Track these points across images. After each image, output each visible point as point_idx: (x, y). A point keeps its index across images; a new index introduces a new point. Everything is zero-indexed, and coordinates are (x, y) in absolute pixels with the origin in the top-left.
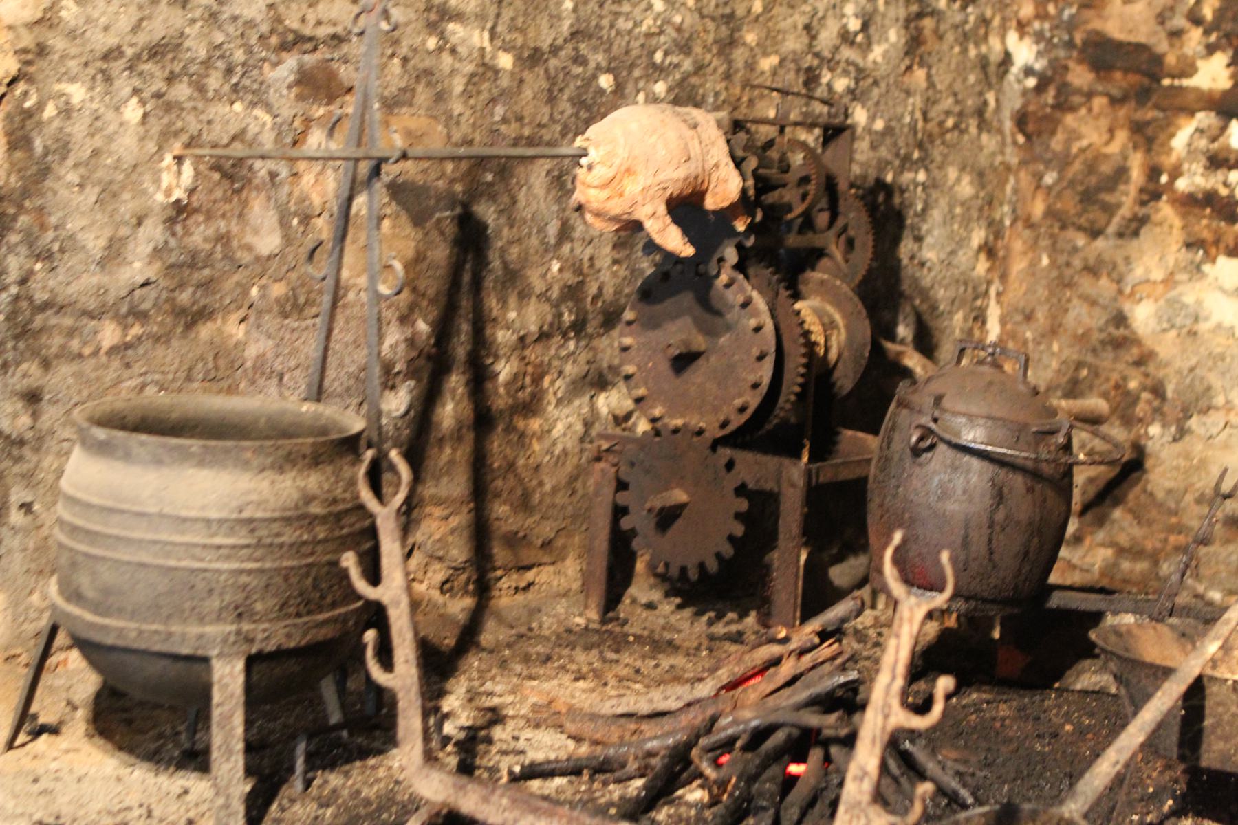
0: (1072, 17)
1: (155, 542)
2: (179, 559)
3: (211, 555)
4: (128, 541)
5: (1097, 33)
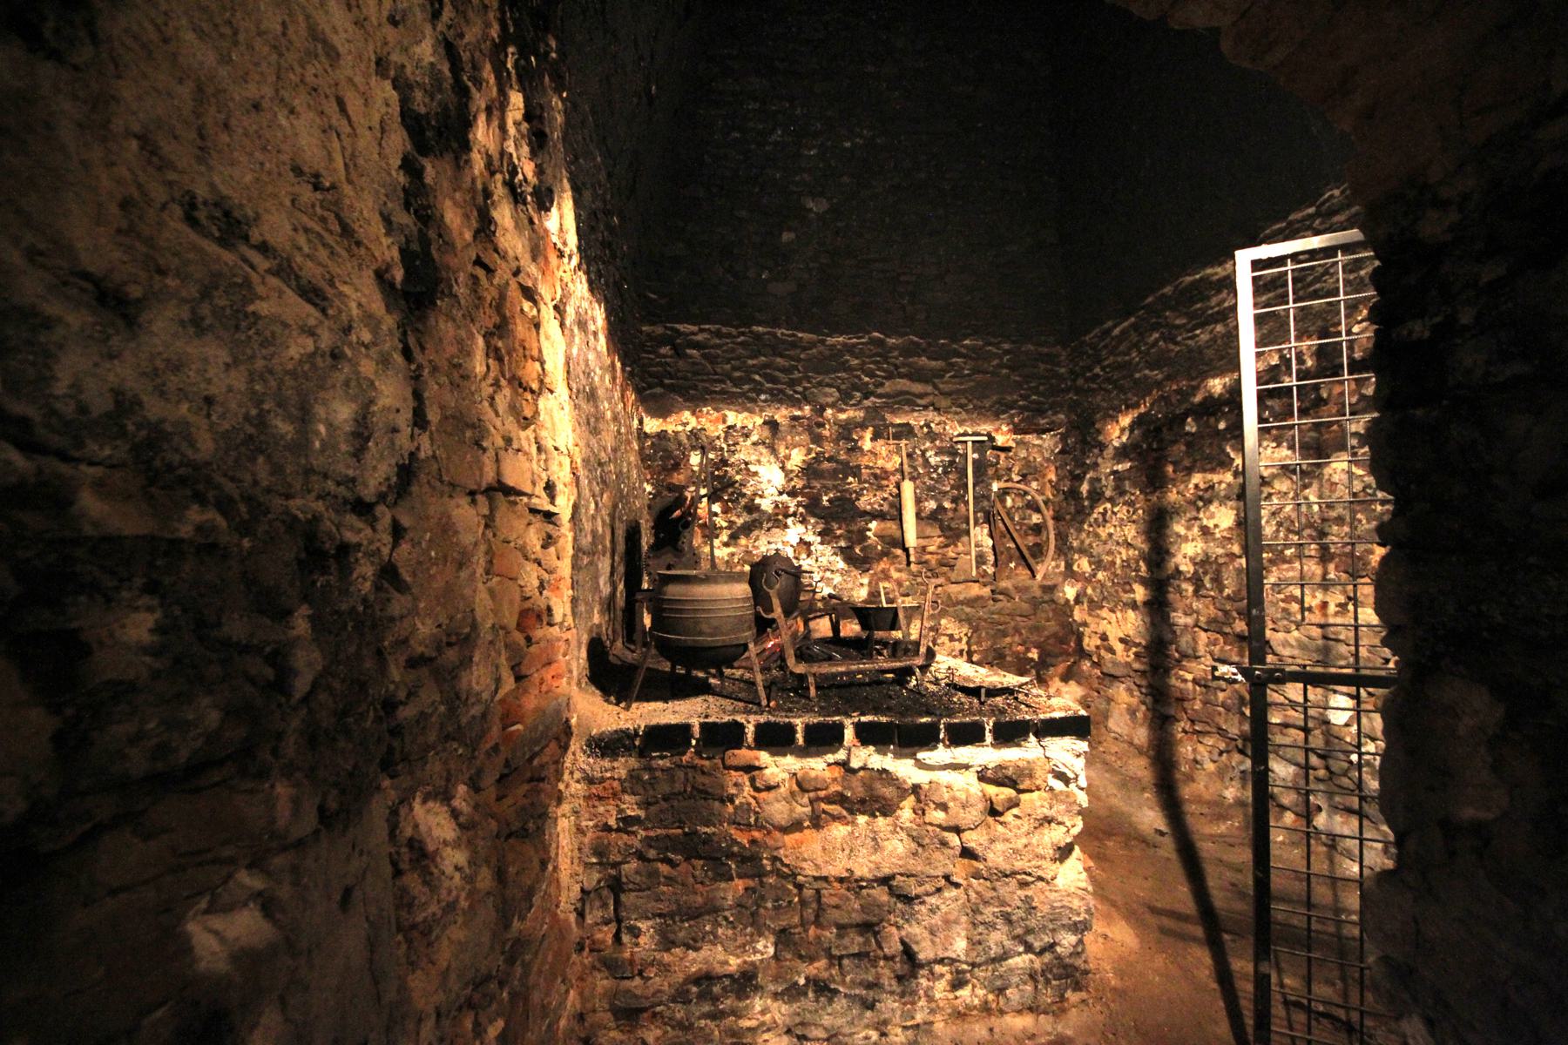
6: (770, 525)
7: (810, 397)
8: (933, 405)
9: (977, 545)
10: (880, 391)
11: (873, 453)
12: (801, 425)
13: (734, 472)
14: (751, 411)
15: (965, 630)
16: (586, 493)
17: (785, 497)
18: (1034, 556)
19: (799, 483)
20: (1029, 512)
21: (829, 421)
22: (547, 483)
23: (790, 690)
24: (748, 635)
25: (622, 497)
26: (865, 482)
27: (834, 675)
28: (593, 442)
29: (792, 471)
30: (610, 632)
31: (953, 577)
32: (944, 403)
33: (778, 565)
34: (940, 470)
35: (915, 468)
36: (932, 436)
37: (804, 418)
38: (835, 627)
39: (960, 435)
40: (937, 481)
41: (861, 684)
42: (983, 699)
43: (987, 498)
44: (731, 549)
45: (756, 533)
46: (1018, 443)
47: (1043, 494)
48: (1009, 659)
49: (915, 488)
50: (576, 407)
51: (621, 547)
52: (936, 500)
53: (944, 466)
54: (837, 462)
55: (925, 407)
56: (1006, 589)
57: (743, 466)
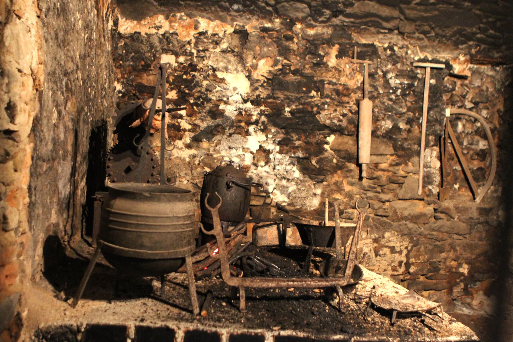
0: (132, 78)
1: (172, 225)
2: (178, 229)
3: (185, 227)
4: (168, 226)
5: (139, 83)
6: (232, 131)
7: (281, 10)
8: (398, 29)
9: (425, 166)
10: (349, 10)
11: (339, 71)
12: (270, 37)
13: (201, 78)
14: (223, 20)
15: (406, 244)
16: (49, 103)
17: (249, 105)
18: (476, 179)
19: (263, 93)
20: (477, 138)
21: (297, 35)
22: (9, 104)
23: (223, 299)
24: (185, 250)
25: (89, 100)
26: (327, 96)
27: (267, 289)
28: (61, 54)
29: (257, 81)
30: (68, 227)
31: (401, 193)
32: (408, 28)
33: (229, 177)
34: (399, 91)
35: (376, 88)
36: (394, 59)
37: (273, 30)
38: (282, 236)
39: (420, 61)
40: (395, 102)
41: (291, 298)
42: (394, 320)
43: (440, 123)
44: (193, 151)
45: (218, 137)
46: (474, 72)
47: (491, 122)
48: (442, 272)
49: (374, 107)
50: (45, 25)
51: (84, 146)
52: (393, 120)
53: (403, 89)
54: (302, 75)
55: (391, 31)
56: (448, 208)
57: (211, 72)
